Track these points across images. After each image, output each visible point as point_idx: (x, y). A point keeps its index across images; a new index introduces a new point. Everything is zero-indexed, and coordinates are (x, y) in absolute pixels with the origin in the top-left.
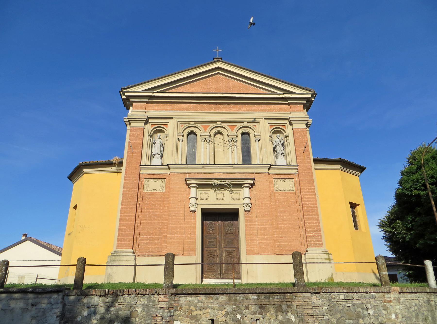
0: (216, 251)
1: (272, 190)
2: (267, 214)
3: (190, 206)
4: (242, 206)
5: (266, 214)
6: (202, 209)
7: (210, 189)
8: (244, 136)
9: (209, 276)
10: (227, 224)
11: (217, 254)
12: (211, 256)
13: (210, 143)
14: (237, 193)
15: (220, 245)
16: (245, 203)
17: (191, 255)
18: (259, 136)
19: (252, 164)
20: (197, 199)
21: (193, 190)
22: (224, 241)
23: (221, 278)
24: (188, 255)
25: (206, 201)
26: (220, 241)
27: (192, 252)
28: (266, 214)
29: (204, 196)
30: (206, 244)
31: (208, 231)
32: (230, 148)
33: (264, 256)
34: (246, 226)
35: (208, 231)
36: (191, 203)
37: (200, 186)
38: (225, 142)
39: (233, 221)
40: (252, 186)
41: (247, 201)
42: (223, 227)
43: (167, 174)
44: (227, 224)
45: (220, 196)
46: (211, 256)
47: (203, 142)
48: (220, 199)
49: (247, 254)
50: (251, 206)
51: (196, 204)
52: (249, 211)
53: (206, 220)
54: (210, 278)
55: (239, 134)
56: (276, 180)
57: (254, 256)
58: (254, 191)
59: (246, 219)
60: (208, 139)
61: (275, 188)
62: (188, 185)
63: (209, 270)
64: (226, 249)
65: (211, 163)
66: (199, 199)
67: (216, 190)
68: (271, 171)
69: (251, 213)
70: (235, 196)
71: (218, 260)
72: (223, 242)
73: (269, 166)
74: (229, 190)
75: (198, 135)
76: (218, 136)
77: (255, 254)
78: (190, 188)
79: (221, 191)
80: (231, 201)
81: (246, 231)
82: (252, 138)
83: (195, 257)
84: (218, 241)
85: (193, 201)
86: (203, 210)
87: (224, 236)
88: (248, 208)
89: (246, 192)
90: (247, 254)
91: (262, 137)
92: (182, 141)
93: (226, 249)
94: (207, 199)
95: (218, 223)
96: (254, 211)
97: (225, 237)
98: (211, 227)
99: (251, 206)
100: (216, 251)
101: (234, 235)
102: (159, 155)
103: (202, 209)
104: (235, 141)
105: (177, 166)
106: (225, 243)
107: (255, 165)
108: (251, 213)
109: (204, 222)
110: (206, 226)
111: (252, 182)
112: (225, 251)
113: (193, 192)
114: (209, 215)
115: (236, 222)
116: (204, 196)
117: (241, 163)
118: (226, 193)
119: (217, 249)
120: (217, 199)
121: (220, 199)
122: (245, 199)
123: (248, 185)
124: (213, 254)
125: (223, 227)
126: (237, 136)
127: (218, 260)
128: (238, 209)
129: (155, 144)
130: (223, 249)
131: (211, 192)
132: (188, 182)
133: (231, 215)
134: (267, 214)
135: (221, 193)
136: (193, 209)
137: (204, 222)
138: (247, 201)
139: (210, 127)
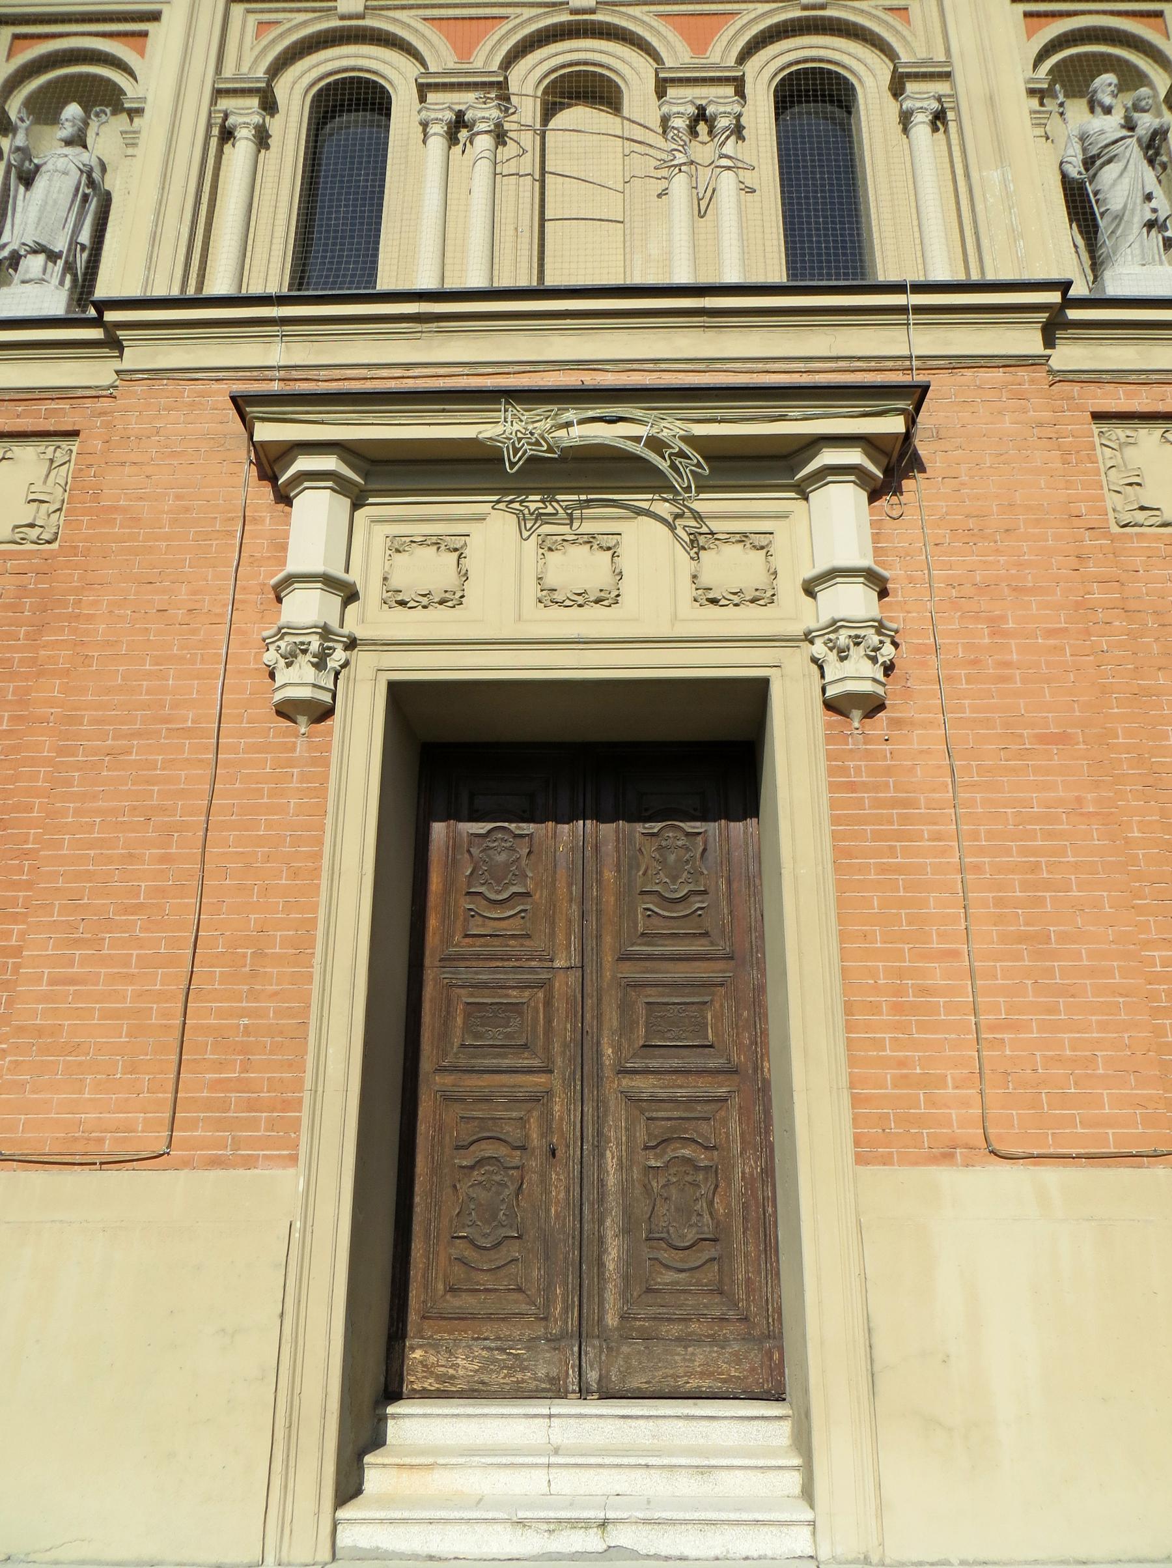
0: (540, 1099)
1: (1093, 519)
2: (1063, 739)
3: (271, 656)
4: (796, 661)
5: (1044, 739)
6: (395, 689)
7: (481, 505)
8: (805, 113)
9: (464, 1365)
10: (650, 848)
11: (547, 1128)
12: (489, 1150)
13: (505, 152)
14: (743, 537)
15: (584, 1044)
16: (834, 625)
17: (249, 1163)
18: (942, 87)
19: (885, 273)
20: (350, 596)
21: (317, 508)
22: (625, 1007)
23: (583, 1393)
24: (216, 1163)
25: (442, 612)
26: (579, 1005)
27: (259, 1131)
28: (1044, 739)
29: (427, 570)
30: (444, 1035)
31: (472, 914)
32: (680, 184)
33: (1051, 1176)
34: (843, 855)
35: (472, 914)
36: (281, 633)
37: (379, 472)
38: (638, 133)
39: (704, 816)
40: (892, 467)
41: (852, 601)
42: (609, 875)
43: (94, 394)
44: (650, 848)
45: (579, 567)
46: (489, 1150)
47: (437, 143)
48: (581, 600)
49: (867, 1152)
50: (888, 651)
51: (326, 633)
52: (873, 706)
53: (453, 814)
54: (475, 1392)
55: (763, 75)
56: (1120, 432)
57: (946, 1176)
58: (912, 515)
59: (841, 783)
60: (483, 112)
61: (1112, 500)
62: (270, 462)
63: (466, 1302)
64: (644, 1085)
65: (505, 281)
66: (372, 592)
67: (539, 517)
68: (1070, 355)
69: (896, 723)
70: (729, 566)
71: (558, 1193)
72: (612, 1018)
73: (1055, 297)
74: (664, 509)
75: (403, 101)
76: (576, 115)
77: (945, 1155)
78: (284, 498)
79: (588, 527)
80: (686, 607)
81: (841, 902)
82: (874, 109)
83: (287, 1182)
84: (560, 1005)
85: (307, 607)
86: (403, 699)
87: (625, 958)
88: (856, 674)
89: (835, 521)
90: (867, 1152)
91: (969, 84)
92: (262, 139)
93: (644, 1085)
94: (450, 600)
95: (566, 835)
96: (914, 702)
97: (630, 971)
98: (498, 876)
99: (888, 651)
100: (540, 1099)
101: (722, 947)
102: (52, 256)
103: (393, 686)
104: (722, 123)
105: (192, 308)
106: (626, 1027)
107: (919, 288)
108: (896, 723)
109: (438, 829)
110: (452, 864)
111: (895, 425)
112: (632, 1099)
113: (315, 524)
114: (467, 757)
115: (737, 827)
116: (427, 570)
117: (777, 274)
118: (645, 543)
119: (556, 1081)
120: (549, 597)
121: (581, 600)
122: (826, 595)
123: (854, 456)
124: (511, 1132)
125: (609, 875)
126: (740, 93)
127: (558, 1193)
128: (754, 695)
129: (27, 180)
130: (613, 1086)
131: (492, 532)
132: (266, 432)
133: (687, 756)
134: (1063, 739)
135: (590, 539)
136: (300, 680)
137: (438, 829)
138: (852, 601)
139: (507, 26)
